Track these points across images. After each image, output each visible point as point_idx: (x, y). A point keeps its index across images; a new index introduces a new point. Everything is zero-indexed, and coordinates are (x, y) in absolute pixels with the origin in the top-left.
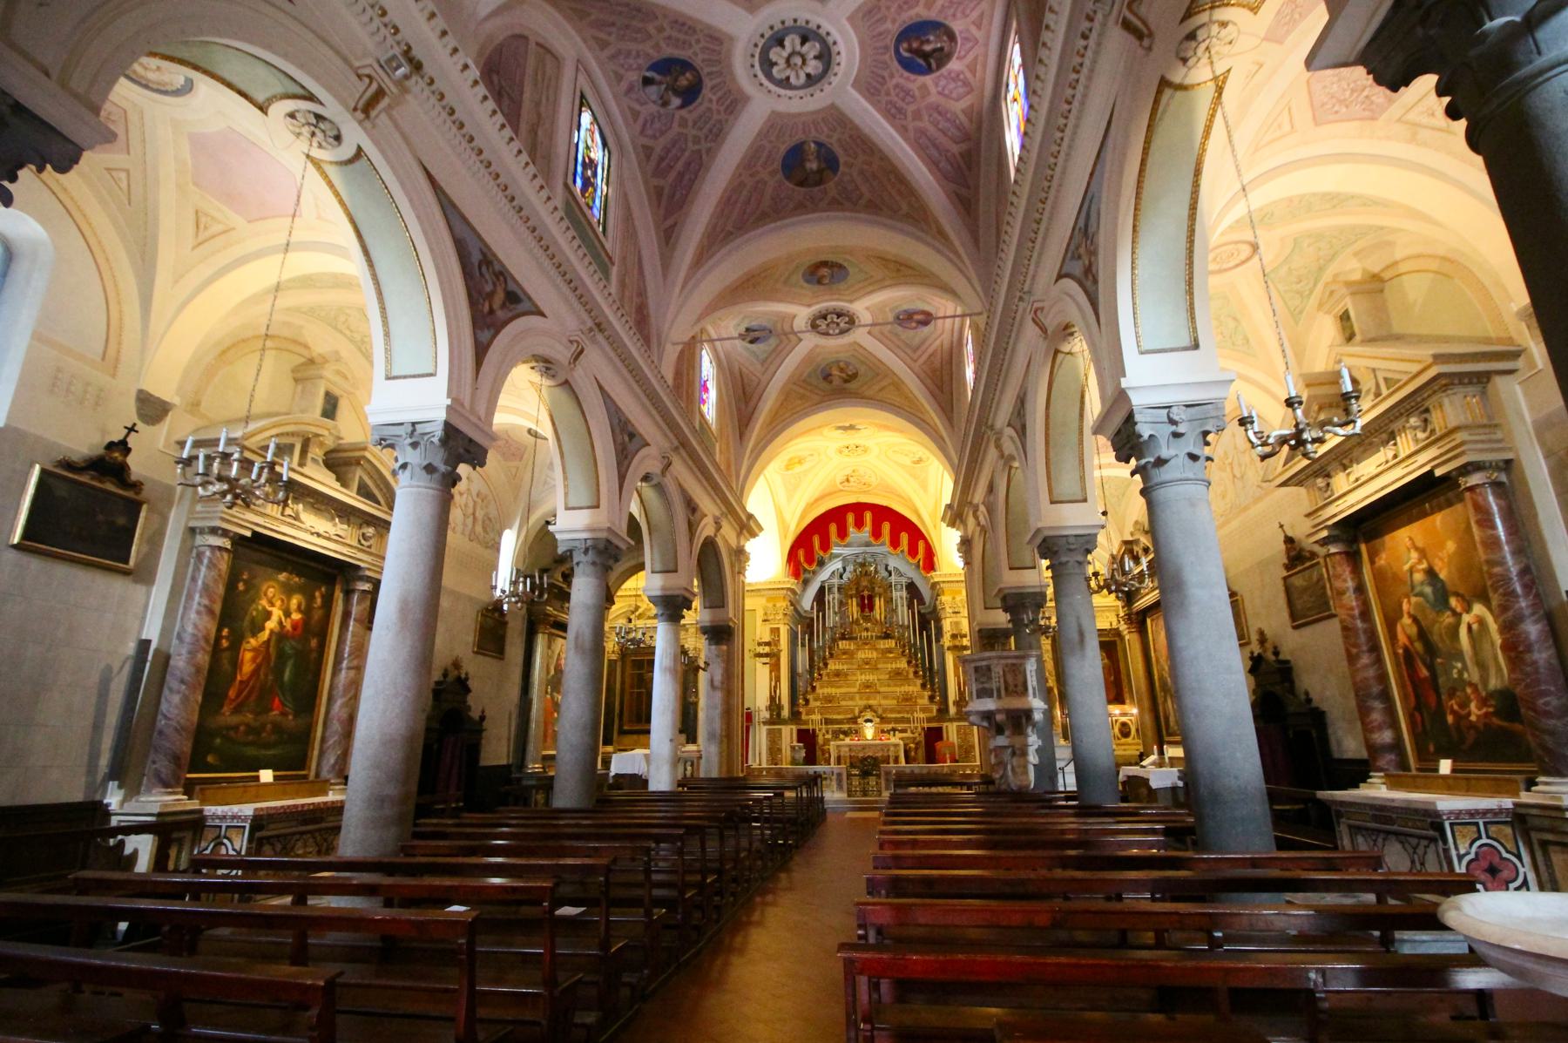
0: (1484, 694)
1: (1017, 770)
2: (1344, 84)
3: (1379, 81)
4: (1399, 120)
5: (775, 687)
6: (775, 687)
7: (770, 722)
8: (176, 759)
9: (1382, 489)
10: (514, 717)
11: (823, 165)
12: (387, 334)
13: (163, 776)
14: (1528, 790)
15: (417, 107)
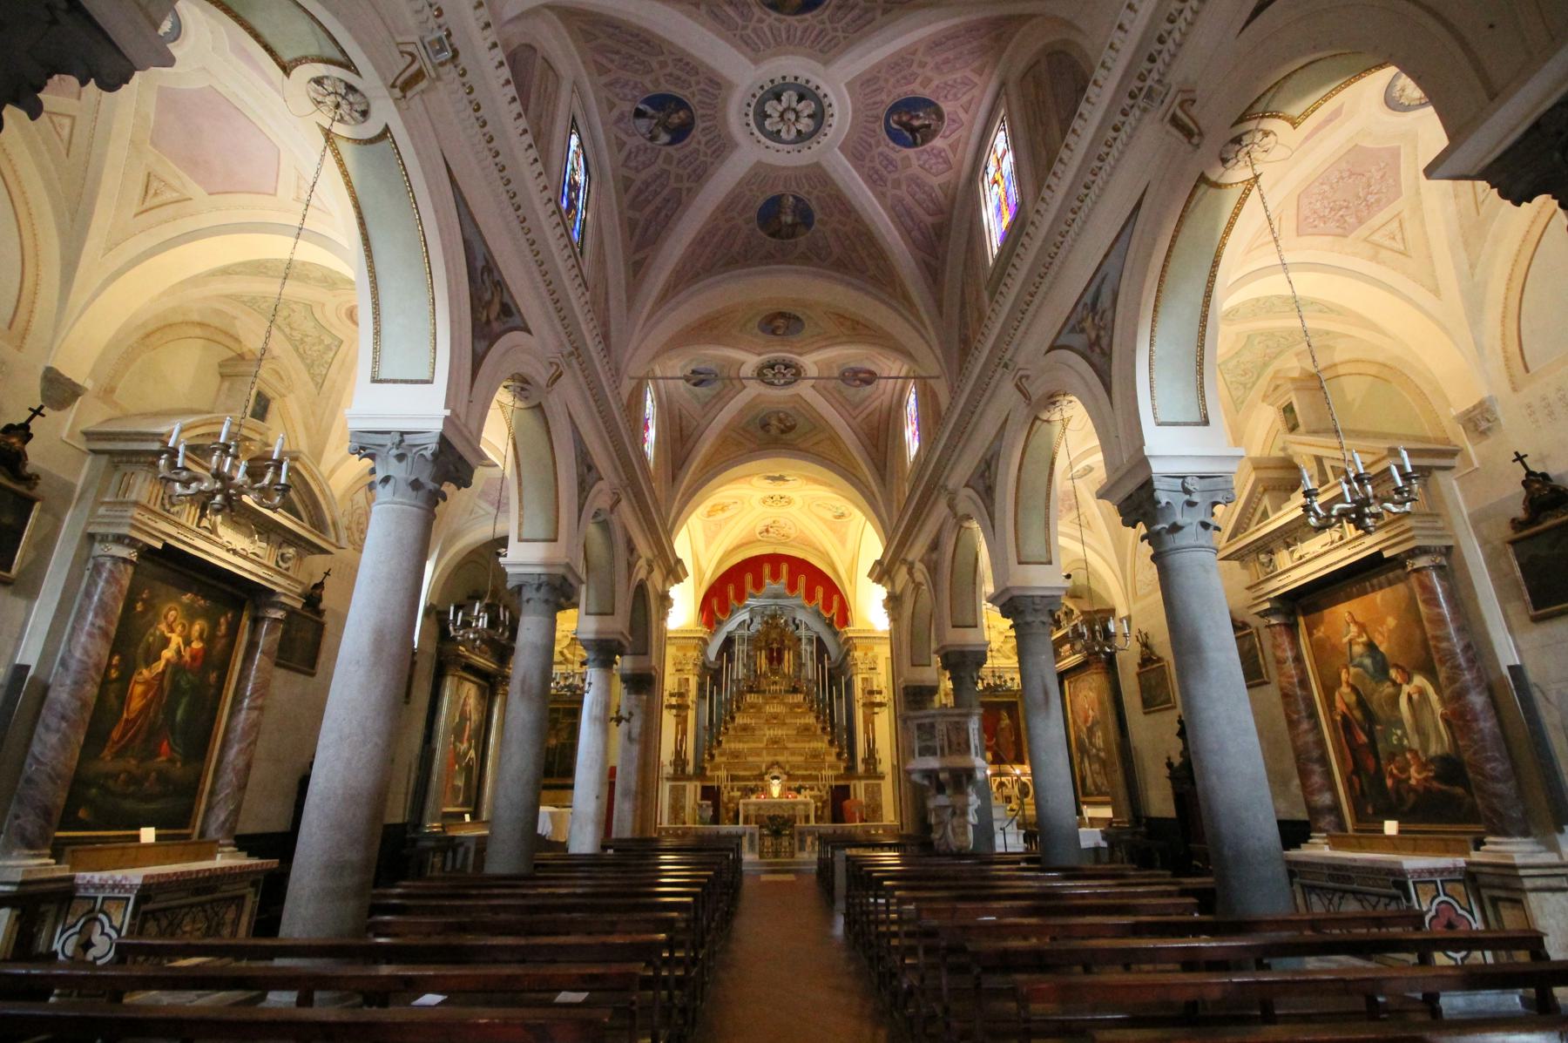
0: (1424, 759)
1: (957, 830)
2: (1326, 202)
3: (1504, 195)
4: (1365, 240)
5: (681, 740)
6: (681, 740)
7: (675, 778)
8: (46, 813)
9: (1327, 567)
10: (414, 768)
11: (798, 220)
12: (377, 333)
13: (27, 834)
14: (1477, 849)
15: (445, 95)
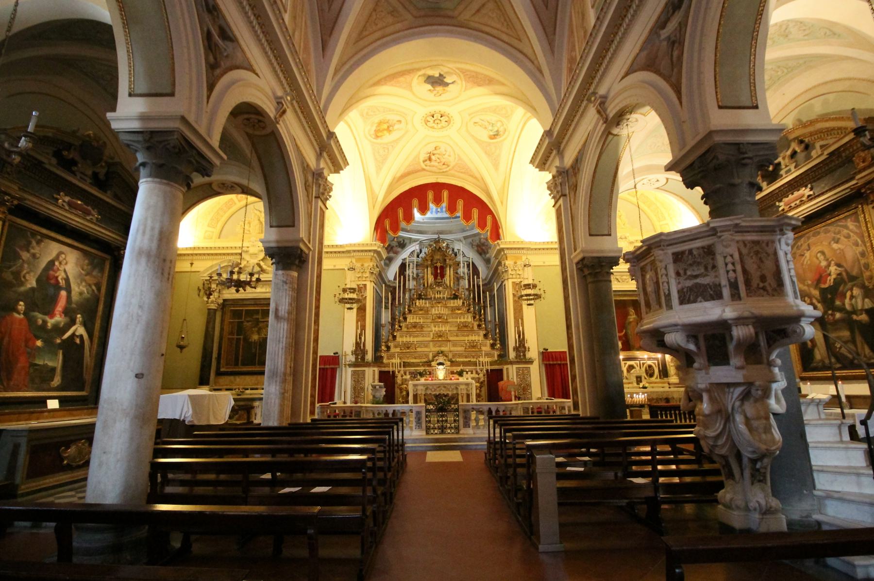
1: (755, 424)
5: (361, 335)
6: (361, 335)
